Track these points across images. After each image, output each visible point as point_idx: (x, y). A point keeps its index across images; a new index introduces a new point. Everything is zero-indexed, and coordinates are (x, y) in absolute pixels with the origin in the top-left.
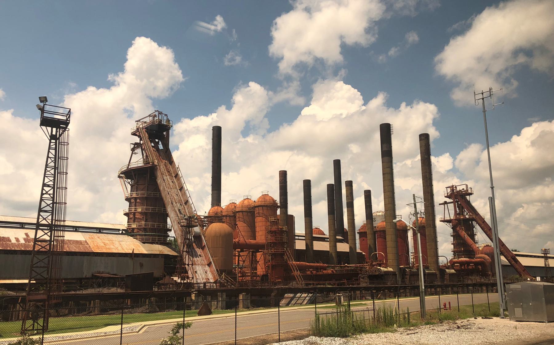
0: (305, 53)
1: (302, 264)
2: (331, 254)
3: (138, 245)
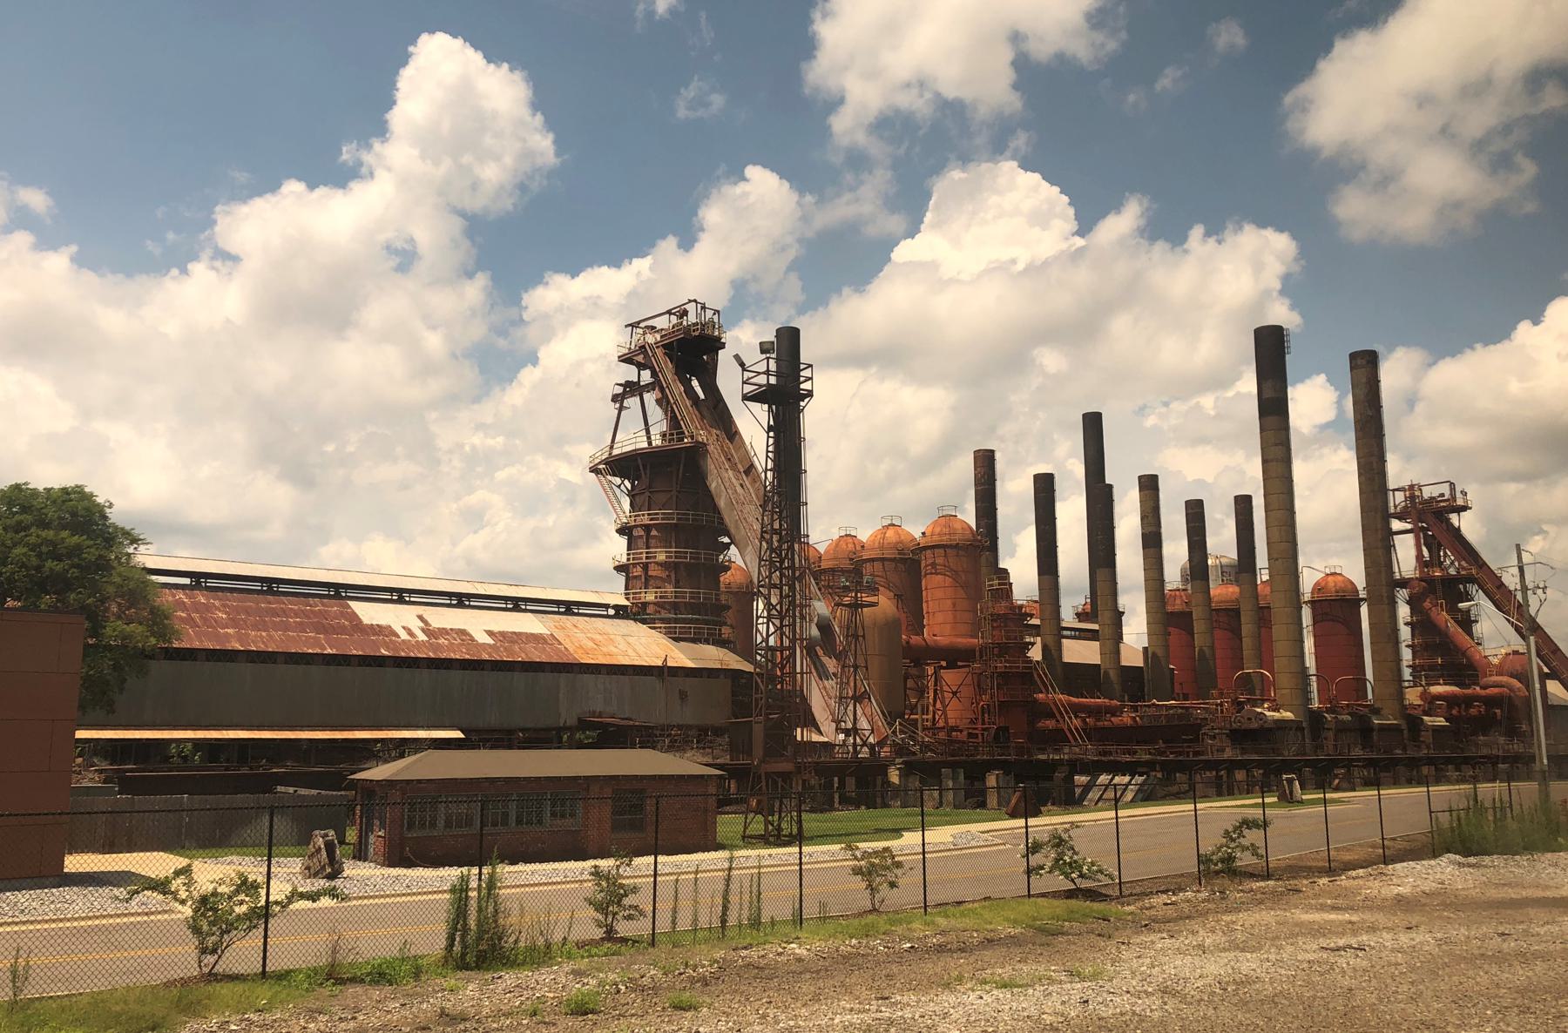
0: (908, 85)
1: (1079, 702)
2: (1106, 673)
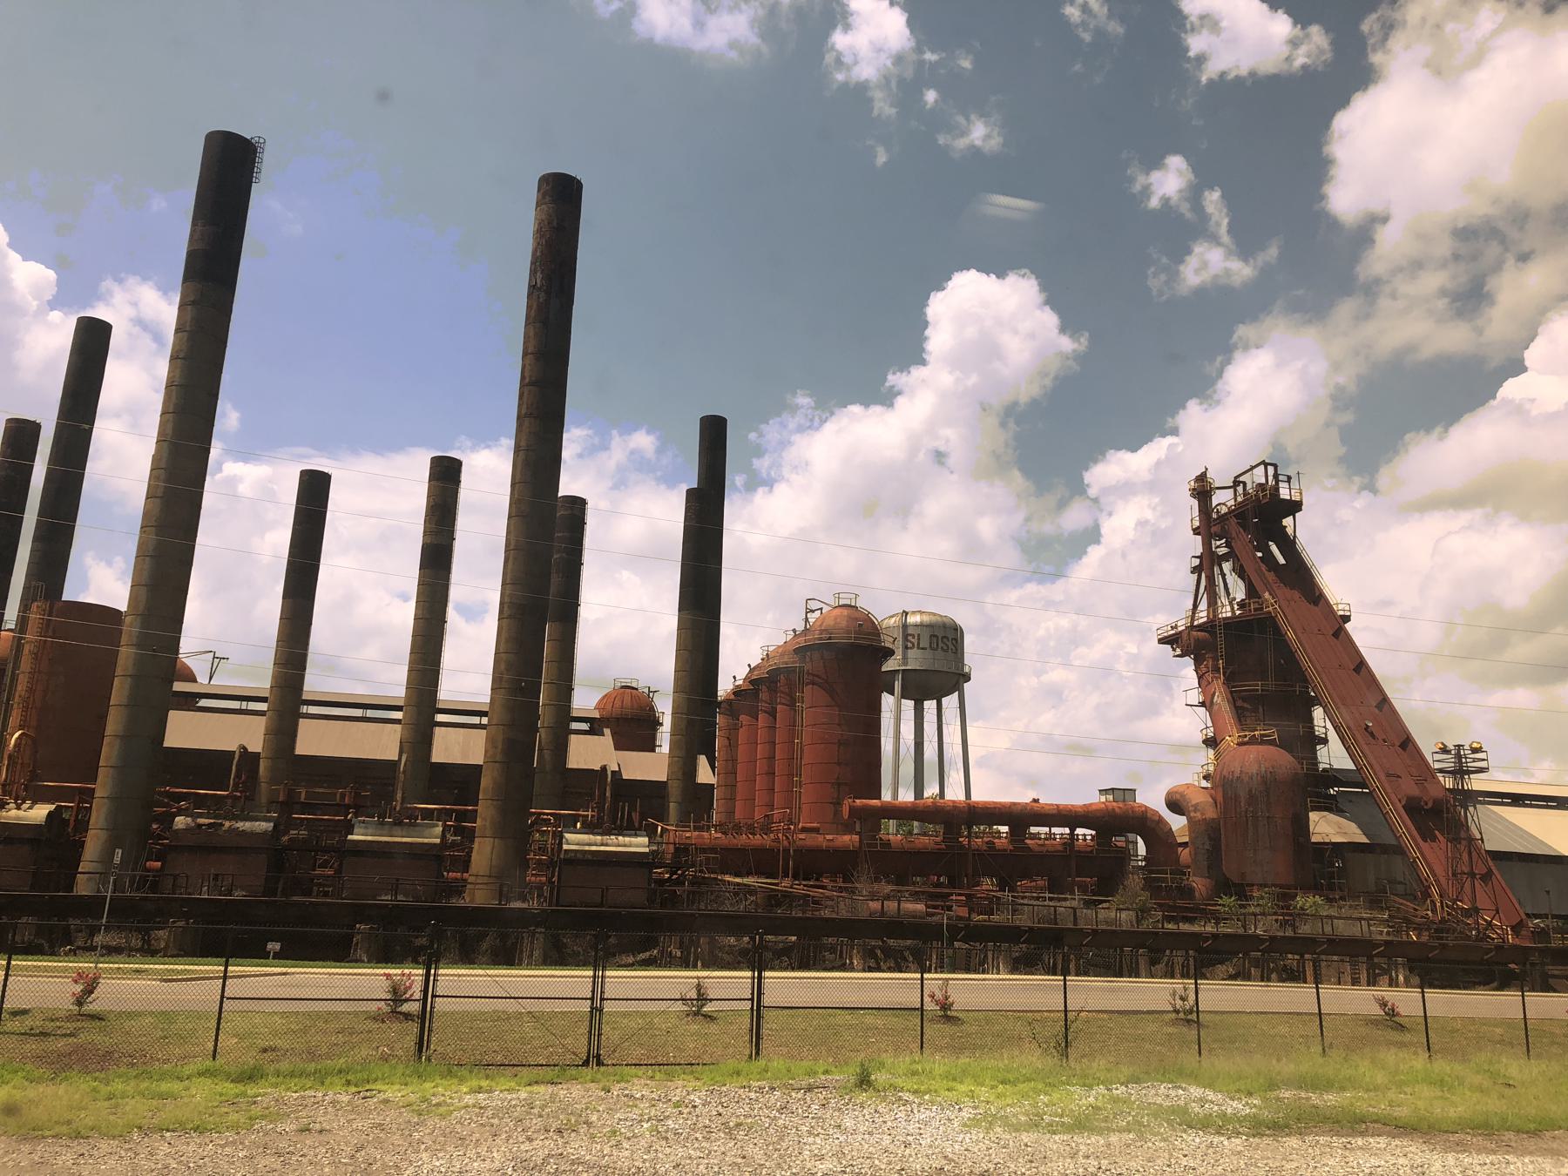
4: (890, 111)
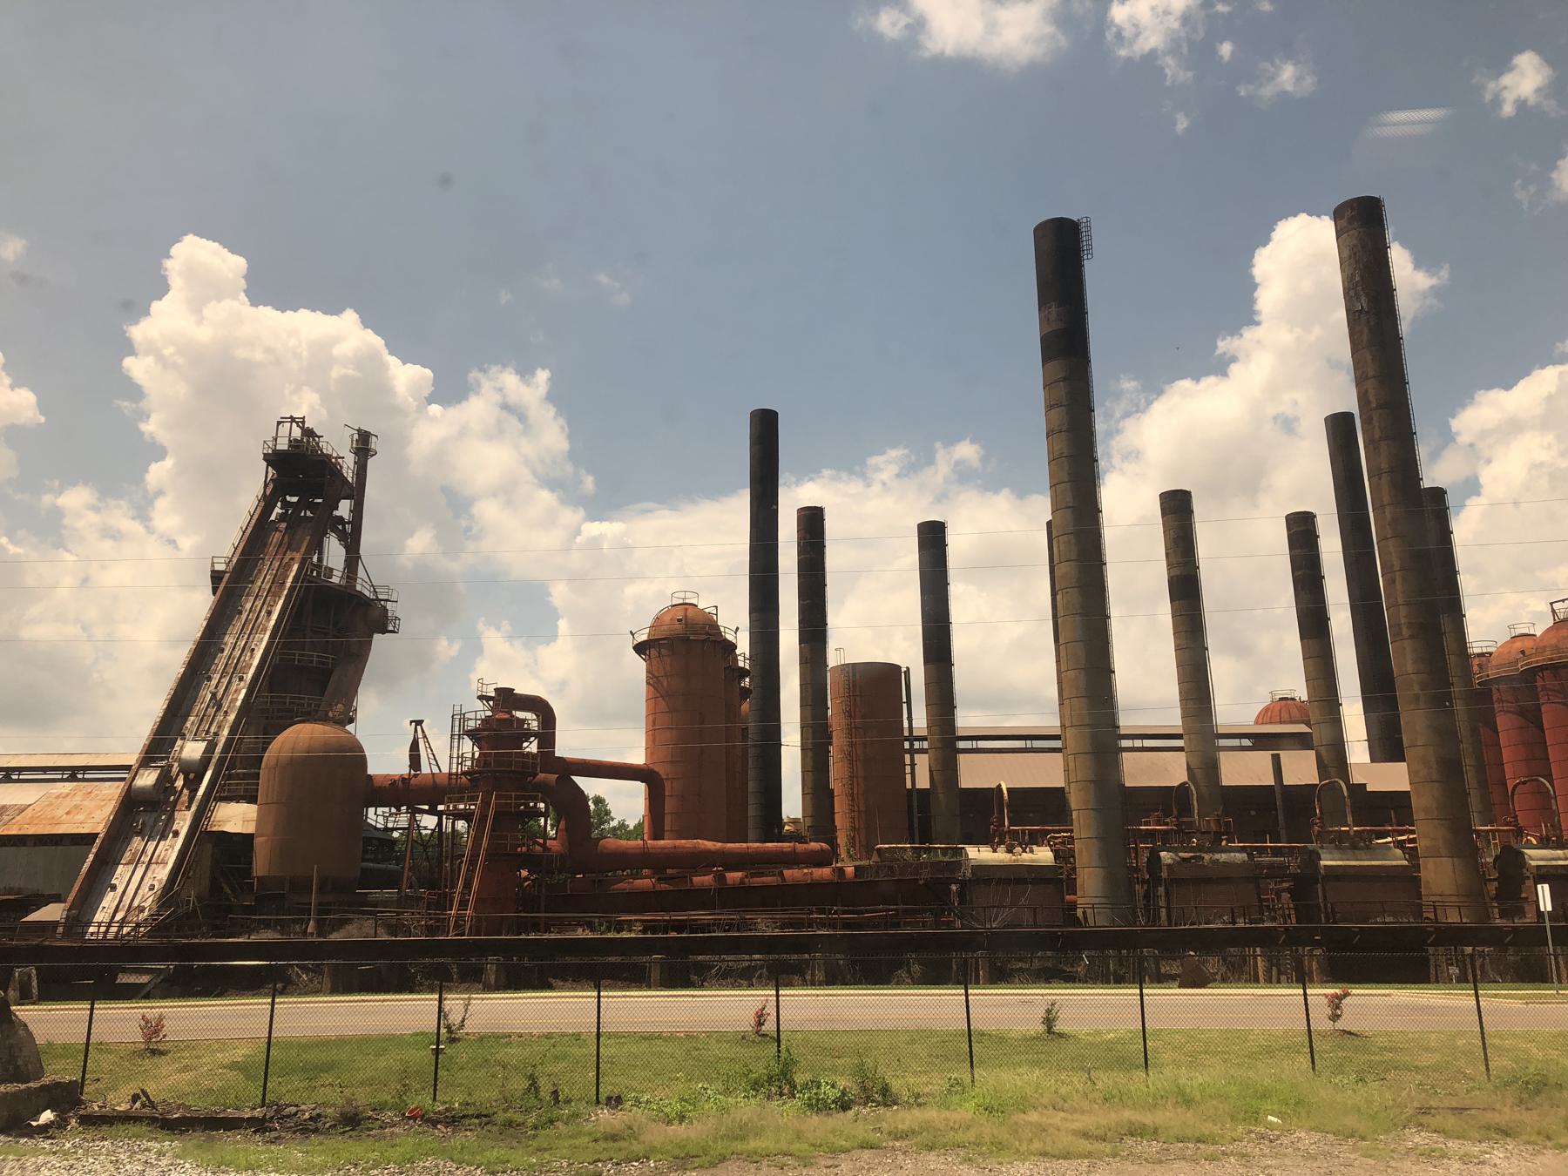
3: (9, 830)
4: (1186, 76)
